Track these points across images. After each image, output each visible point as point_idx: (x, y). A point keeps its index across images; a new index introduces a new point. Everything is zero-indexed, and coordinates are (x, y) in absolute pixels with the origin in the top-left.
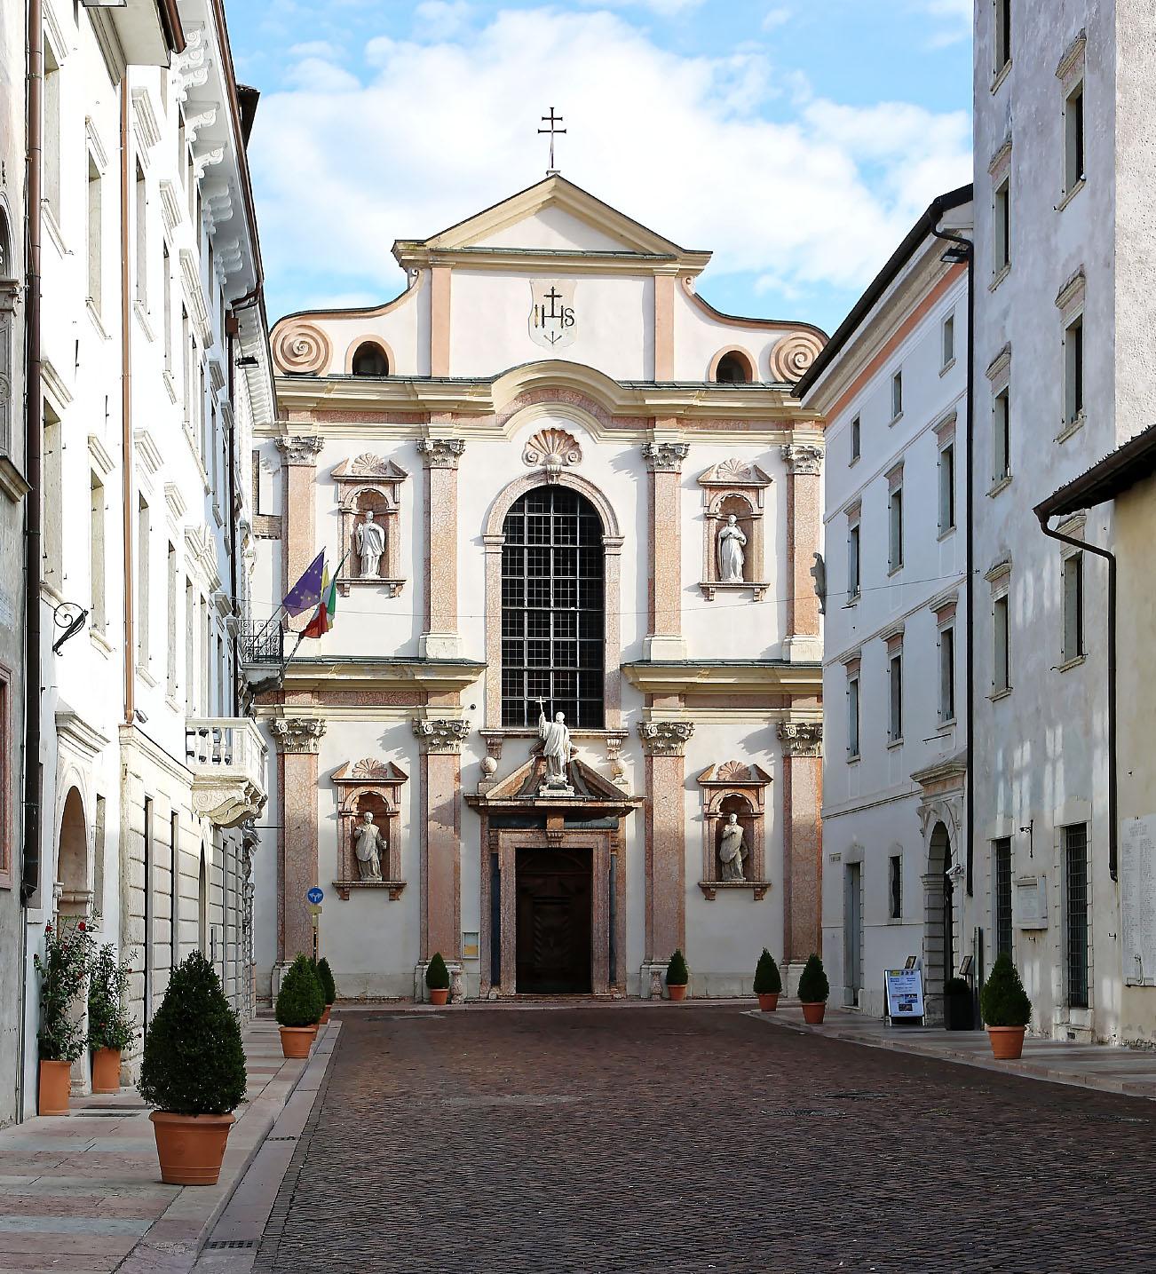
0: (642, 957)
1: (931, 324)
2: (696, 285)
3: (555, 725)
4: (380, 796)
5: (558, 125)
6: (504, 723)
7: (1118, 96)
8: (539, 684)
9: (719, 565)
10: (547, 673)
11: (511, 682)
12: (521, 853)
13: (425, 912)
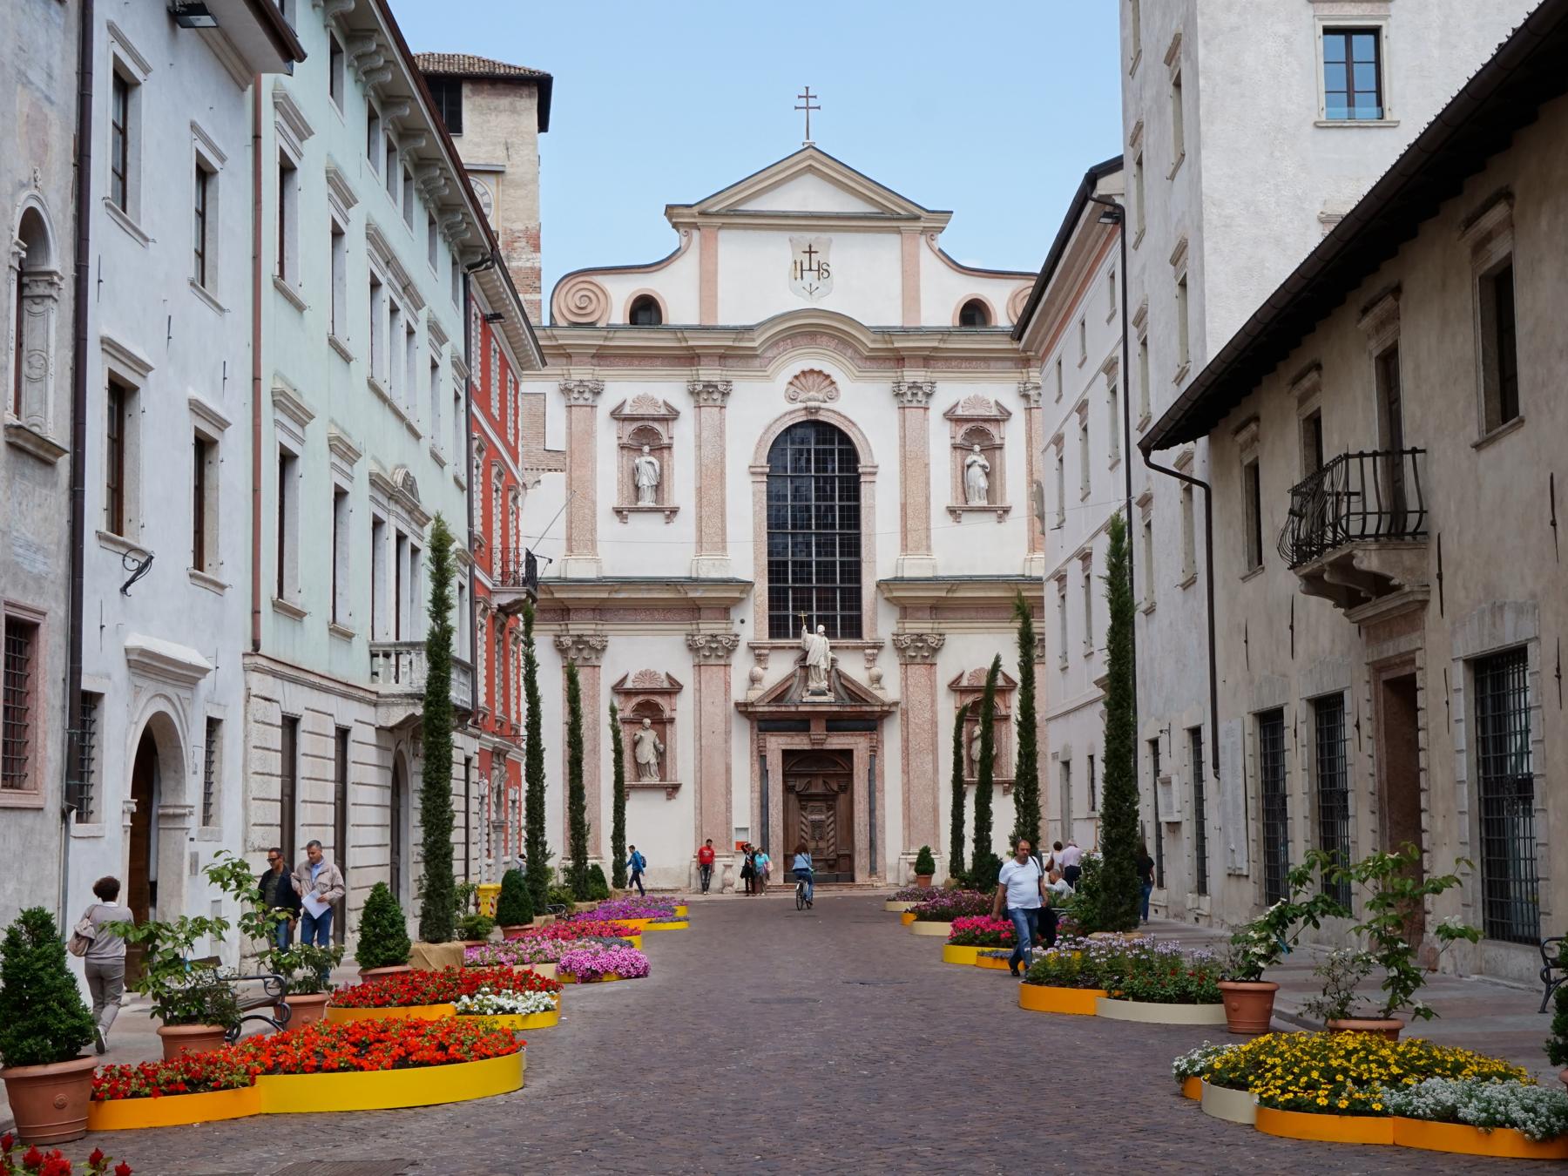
0: (900, 849)
1: (1100, 281)
2: (942, 241)
3: (815, 636)
4: (657, 705)
5: (812, 102)
6: (771, 636)
7: (1202, 82)
8: (802, 600)
9: (965, 489)
10: (786, 590)
11: (776, 599)
12: (787, 754)
13: (700, 810)
